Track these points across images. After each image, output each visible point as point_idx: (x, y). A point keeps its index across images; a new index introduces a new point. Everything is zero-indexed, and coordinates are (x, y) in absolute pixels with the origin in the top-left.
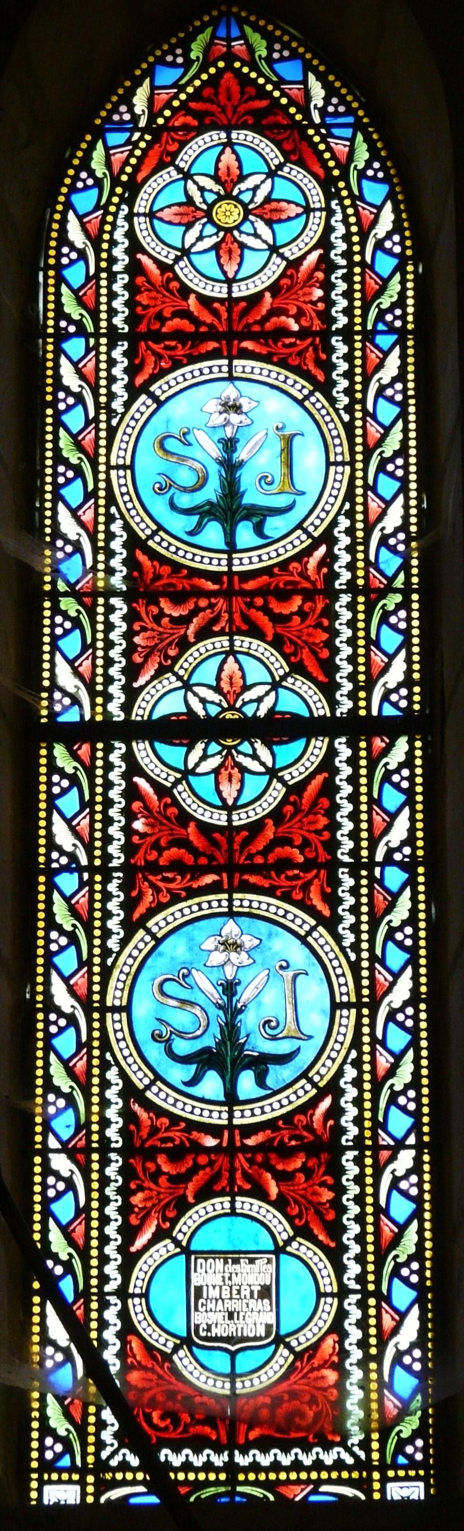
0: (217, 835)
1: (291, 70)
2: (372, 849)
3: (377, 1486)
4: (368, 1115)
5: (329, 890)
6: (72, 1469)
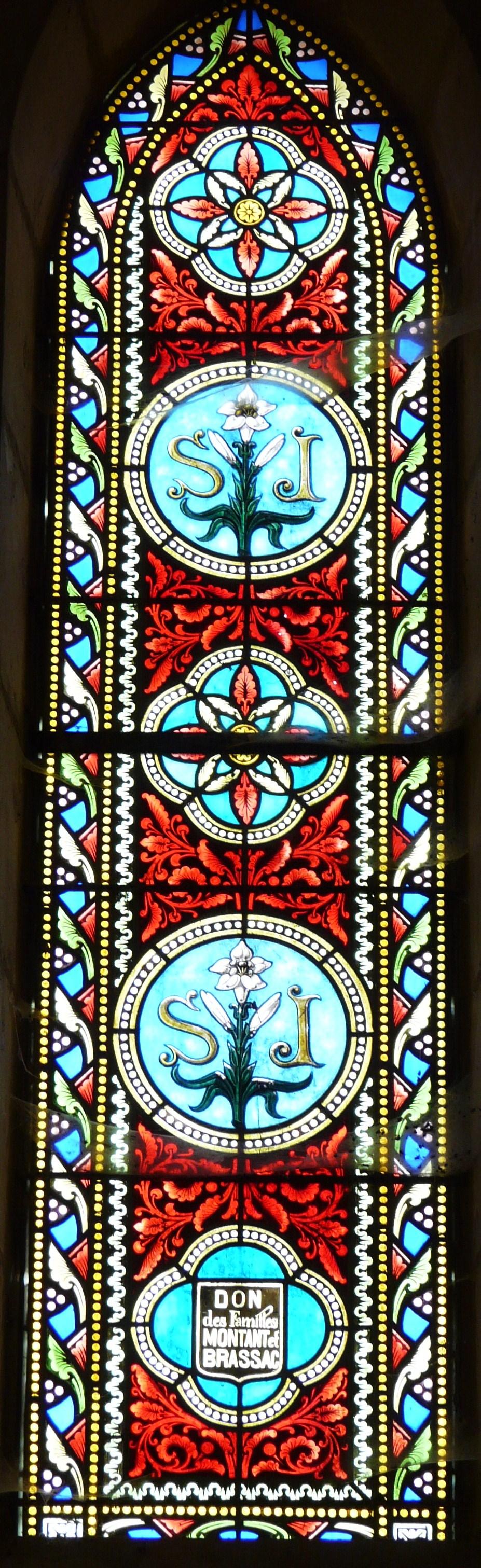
0: (234, 305)
1: (315, 70)
2: (391, 874)
5: (347, 916)
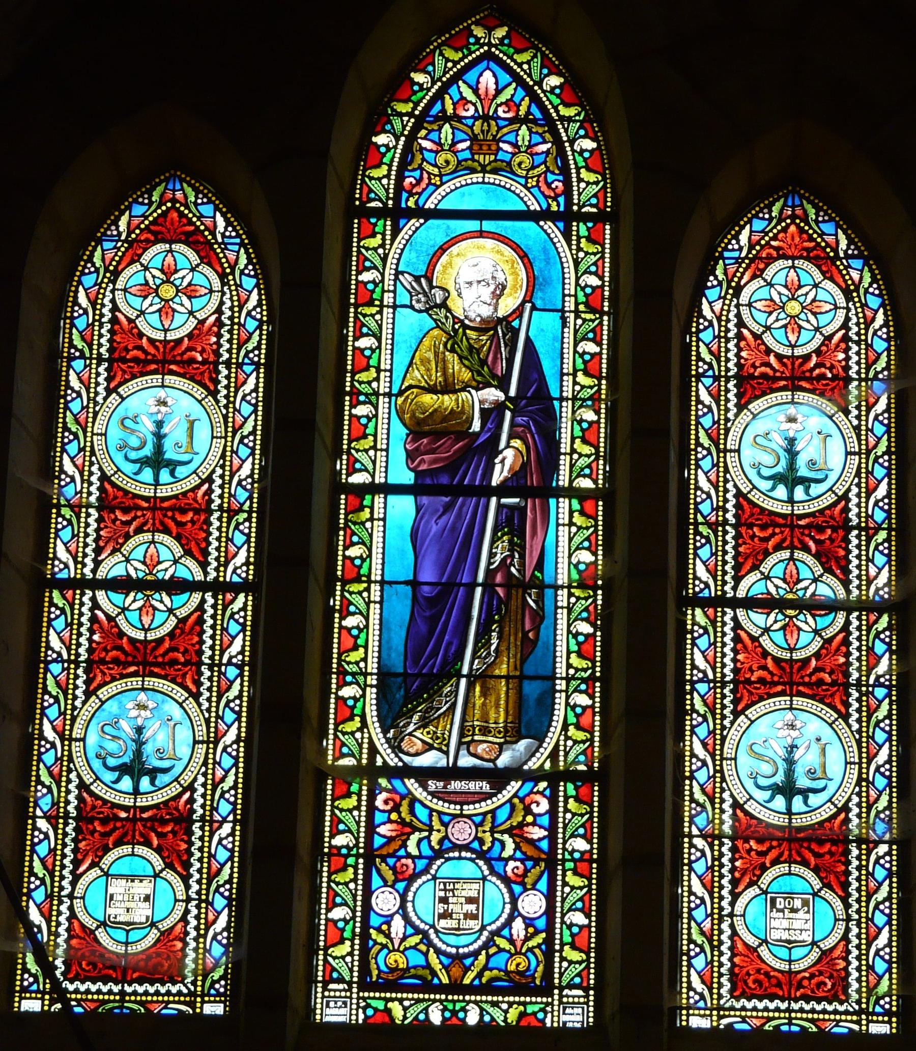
2: (868, 676)
6: (38, 991)
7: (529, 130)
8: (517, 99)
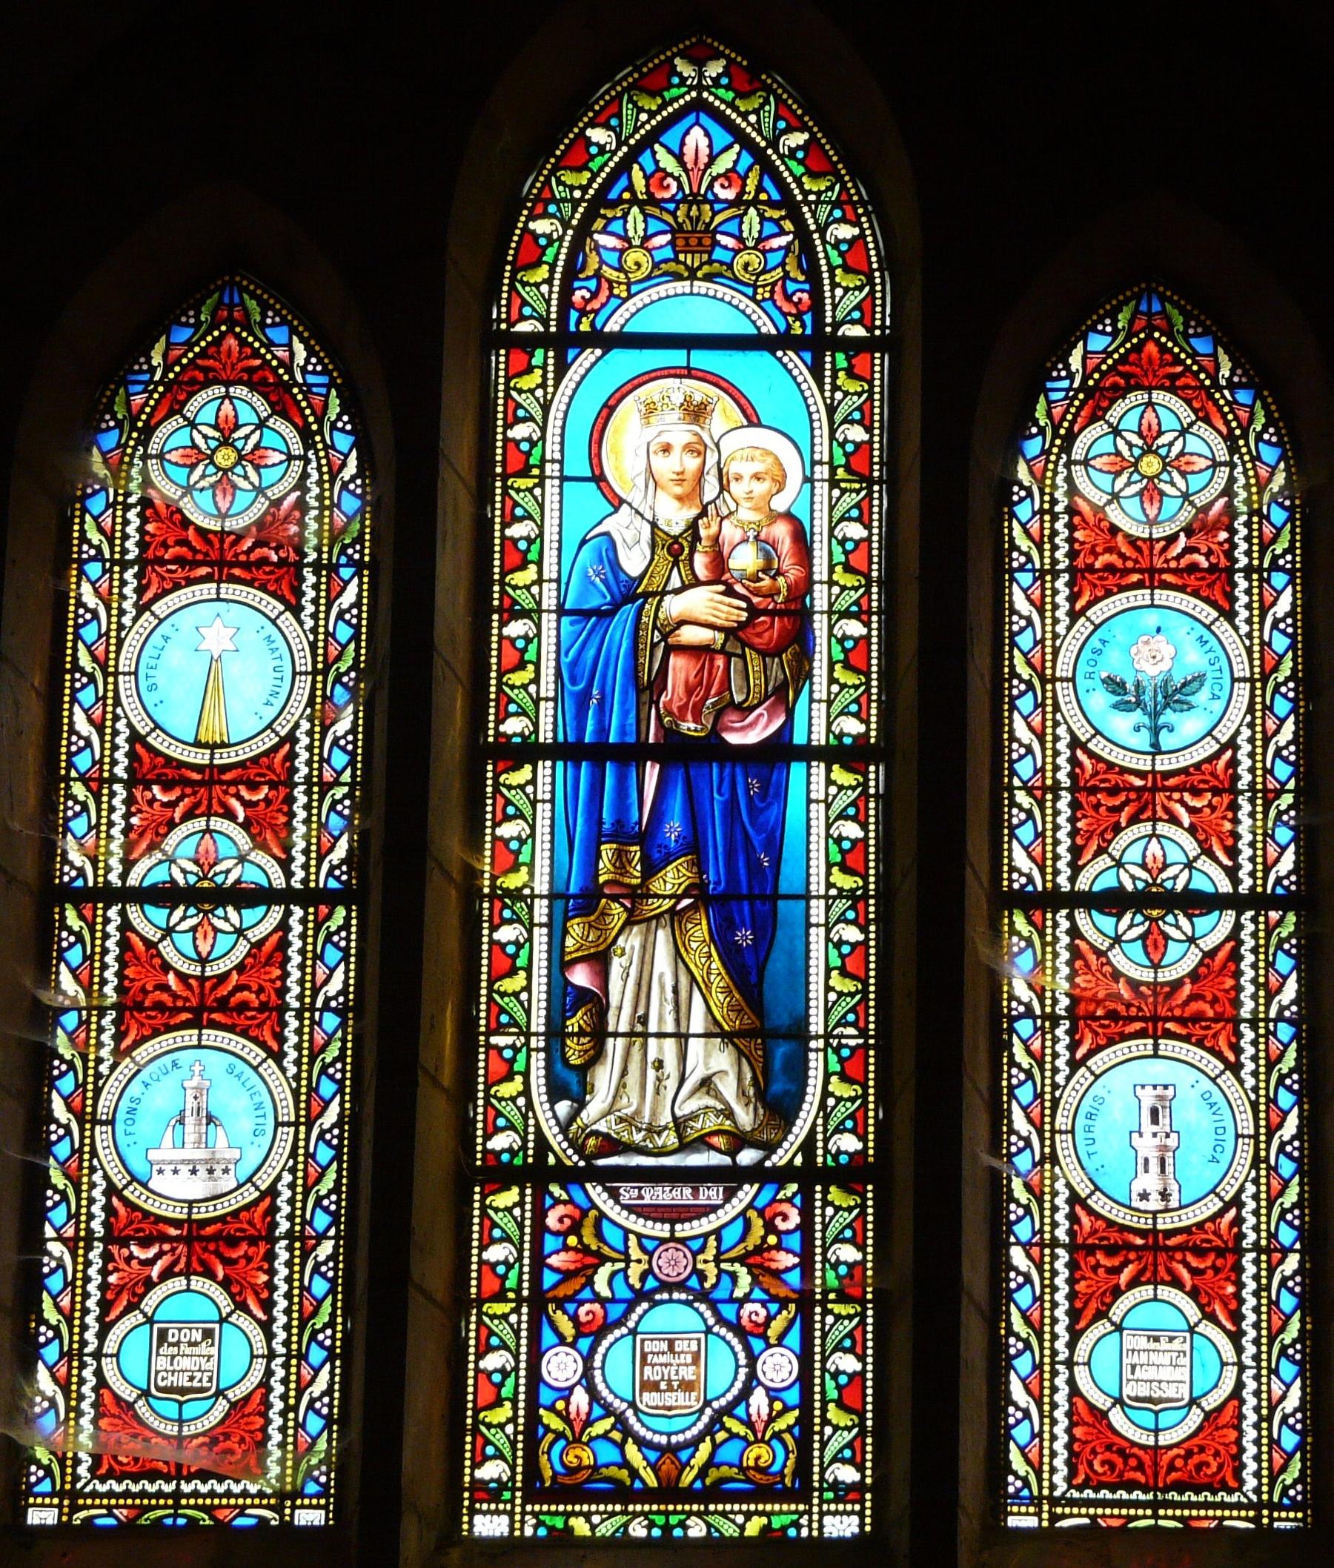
3: (287, 1511)
4: (298, 1212)
7: (761, 215)
8: (741, 168)
